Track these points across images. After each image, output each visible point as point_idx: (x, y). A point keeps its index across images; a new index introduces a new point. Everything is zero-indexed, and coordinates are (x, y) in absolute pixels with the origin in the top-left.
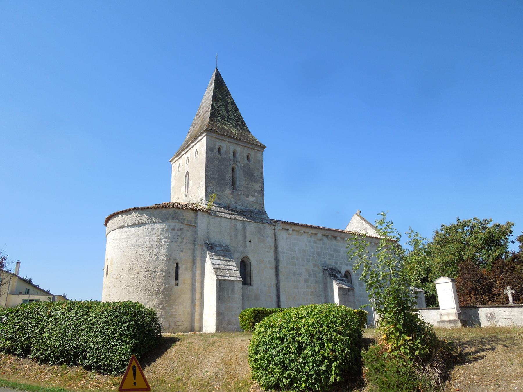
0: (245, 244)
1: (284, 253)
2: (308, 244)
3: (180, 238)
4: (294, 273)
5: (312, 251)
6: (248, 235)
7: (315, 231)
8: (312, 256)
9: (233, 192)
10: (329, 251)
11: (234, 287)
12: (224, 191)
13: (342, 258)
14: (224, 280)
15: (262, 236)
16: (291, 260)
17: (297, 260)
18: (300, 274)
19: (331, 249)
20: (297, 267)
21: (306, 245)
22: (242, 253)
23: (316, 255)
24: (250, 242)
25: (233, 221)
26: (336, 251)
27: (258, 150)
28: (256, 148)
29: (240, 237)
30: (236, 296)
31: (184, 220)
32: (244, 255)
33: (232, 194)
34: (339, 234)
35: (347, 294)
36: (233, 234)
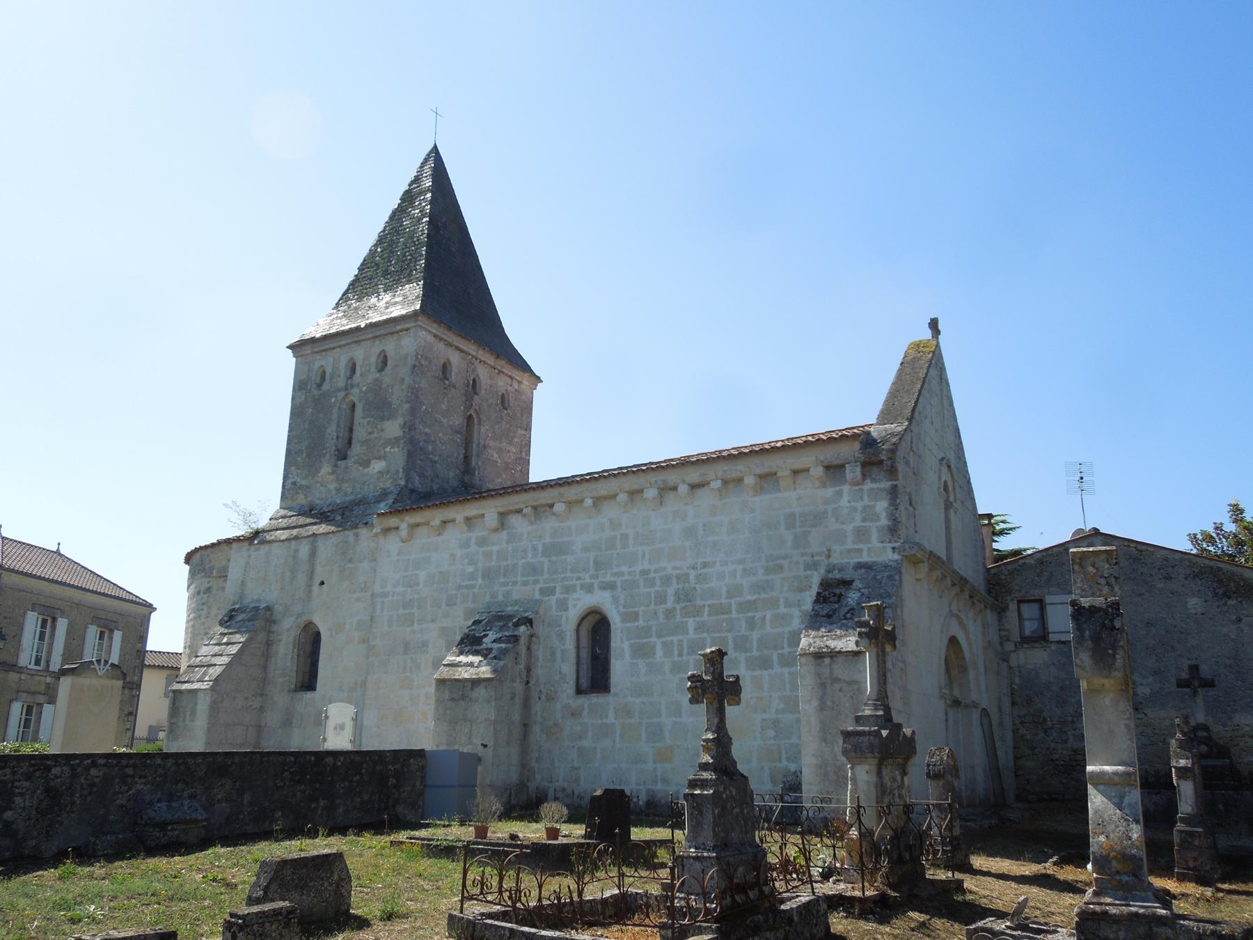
0: (310, 591)
1: (385, 595)
2: (459, 553)
3: (205, 608)
4: (406, 647)
5: (471, 569)
6: (318, 569)
7: (694, 475)
8: (468, 587)
9: (336, 466)
10: (530, 559)
11: (196, 704)
12: (318, 471)
13: (573, 571)
14: (180, 692)
15: (350, 561)
16: (401, 611)
17: (419, 607)
18: (424, 645)
19: (535, 549)
20: (416, 626)
21: (453, 556)
22: (299, 616)
23: (480, 581)
24: (322, 583)
25: (293, 542)
26: (556, 549)
27: (407, 330)
28: (398, 328)
29: (301, 578)
30: (198, 723)
31: (212, 569)
32: (305, 618)
33: (333, 473)
34: (556, 491)
35: (463, 697)
36: (288, 574)
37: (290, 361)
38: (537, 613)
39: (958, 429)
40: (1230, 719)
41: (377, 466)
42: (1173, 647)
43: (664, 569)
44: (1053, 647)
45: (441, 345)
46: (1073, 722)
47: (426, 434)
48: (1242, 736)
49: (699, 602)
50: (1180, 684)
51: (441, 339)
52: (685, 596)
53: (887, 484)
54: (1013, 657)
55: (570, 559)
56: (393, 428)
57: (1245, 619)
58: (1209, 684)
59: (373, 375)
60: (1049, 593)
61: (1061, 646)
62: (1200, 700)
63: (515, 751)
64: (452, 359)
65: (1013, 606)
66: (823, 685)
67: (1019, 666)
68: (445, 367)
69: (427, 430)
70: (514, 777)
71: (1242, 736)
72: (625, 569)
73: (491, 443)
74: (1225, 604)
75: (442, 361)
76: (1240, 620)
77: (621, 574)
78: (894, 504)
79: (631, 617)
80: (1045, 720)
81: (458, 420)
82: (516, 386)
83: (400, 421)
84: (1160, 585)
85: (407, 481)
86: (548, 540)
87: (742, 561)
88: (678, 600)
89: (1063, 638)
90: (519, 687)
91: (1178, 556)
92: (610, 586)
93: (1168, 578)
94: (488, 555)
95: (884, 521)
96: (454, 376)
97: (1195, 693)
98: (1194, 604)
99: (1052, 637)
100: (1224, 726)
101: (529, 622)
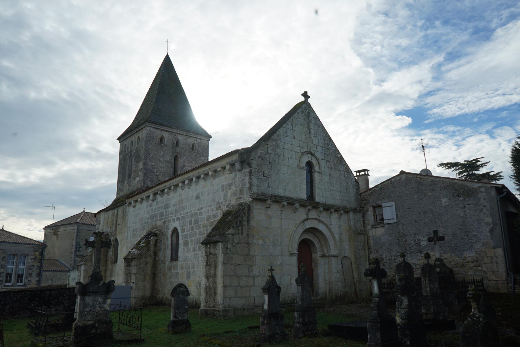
37: (118, 144)
38: (160, 231)
39: (329, 136)
40: (462, 254)
41: (137, 179)
42: (435, 222)
43: (191, 211)
44: (386, 226)
45: (159, 131)
46: (395, 259)
47: (153, 165)
48: (468, 262)
49: (200, 223)
50: (430, 240)
51: (158, 129)
52: (196, 222)
53: (248, 170)
54: (371, 232)
55: (170, 209)
56: (141, 165)
57: (467, 206)
58: (443, 238)
59: (136, 146)
60: (384, 202)
61: (389, 225)
62: (437, 247)
63: (148, 285)
64: (164, 135)
65: (371, 209)
66: (207, 256)
67: (373, 236)
68: (162, 139)
69: (153, 164)
70: (148, 293)
71: (468, 262)
72: (182, 212)
73: (187, 165)
74: (458, 200)
75: (160, 137)
76: (464, 207)
77: (181, 214)
78: (250, 177)
79: (183, 231)
80: (383, 259)
81: (169, 157)
82: (199, 141)
83: (142, 162)
84: (430, 194)
85: (144, 184)
86: (165, 203)
87: (210, 206)
88: (195, 223)
89: (390, 222)
90: (150, 260)
91: (438, 179)
92: (178, 219)
93: (433, 190)
94: (152, 210)
95: (248, 185)
96: (165, 142)
97: (435, 244)
98: (444, 201)
99: (385, 222)
100: (459, 258)
101: (156, 235)
